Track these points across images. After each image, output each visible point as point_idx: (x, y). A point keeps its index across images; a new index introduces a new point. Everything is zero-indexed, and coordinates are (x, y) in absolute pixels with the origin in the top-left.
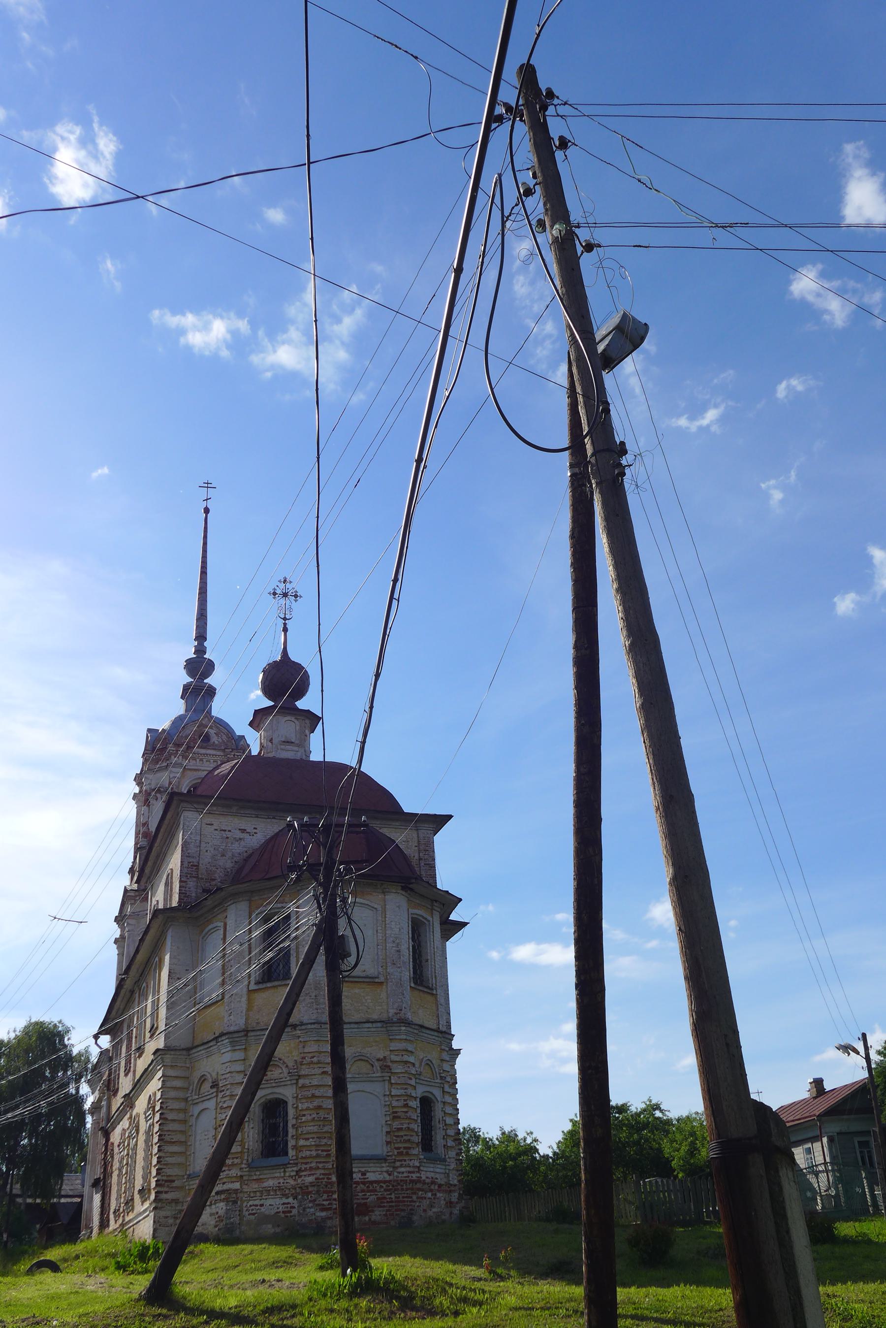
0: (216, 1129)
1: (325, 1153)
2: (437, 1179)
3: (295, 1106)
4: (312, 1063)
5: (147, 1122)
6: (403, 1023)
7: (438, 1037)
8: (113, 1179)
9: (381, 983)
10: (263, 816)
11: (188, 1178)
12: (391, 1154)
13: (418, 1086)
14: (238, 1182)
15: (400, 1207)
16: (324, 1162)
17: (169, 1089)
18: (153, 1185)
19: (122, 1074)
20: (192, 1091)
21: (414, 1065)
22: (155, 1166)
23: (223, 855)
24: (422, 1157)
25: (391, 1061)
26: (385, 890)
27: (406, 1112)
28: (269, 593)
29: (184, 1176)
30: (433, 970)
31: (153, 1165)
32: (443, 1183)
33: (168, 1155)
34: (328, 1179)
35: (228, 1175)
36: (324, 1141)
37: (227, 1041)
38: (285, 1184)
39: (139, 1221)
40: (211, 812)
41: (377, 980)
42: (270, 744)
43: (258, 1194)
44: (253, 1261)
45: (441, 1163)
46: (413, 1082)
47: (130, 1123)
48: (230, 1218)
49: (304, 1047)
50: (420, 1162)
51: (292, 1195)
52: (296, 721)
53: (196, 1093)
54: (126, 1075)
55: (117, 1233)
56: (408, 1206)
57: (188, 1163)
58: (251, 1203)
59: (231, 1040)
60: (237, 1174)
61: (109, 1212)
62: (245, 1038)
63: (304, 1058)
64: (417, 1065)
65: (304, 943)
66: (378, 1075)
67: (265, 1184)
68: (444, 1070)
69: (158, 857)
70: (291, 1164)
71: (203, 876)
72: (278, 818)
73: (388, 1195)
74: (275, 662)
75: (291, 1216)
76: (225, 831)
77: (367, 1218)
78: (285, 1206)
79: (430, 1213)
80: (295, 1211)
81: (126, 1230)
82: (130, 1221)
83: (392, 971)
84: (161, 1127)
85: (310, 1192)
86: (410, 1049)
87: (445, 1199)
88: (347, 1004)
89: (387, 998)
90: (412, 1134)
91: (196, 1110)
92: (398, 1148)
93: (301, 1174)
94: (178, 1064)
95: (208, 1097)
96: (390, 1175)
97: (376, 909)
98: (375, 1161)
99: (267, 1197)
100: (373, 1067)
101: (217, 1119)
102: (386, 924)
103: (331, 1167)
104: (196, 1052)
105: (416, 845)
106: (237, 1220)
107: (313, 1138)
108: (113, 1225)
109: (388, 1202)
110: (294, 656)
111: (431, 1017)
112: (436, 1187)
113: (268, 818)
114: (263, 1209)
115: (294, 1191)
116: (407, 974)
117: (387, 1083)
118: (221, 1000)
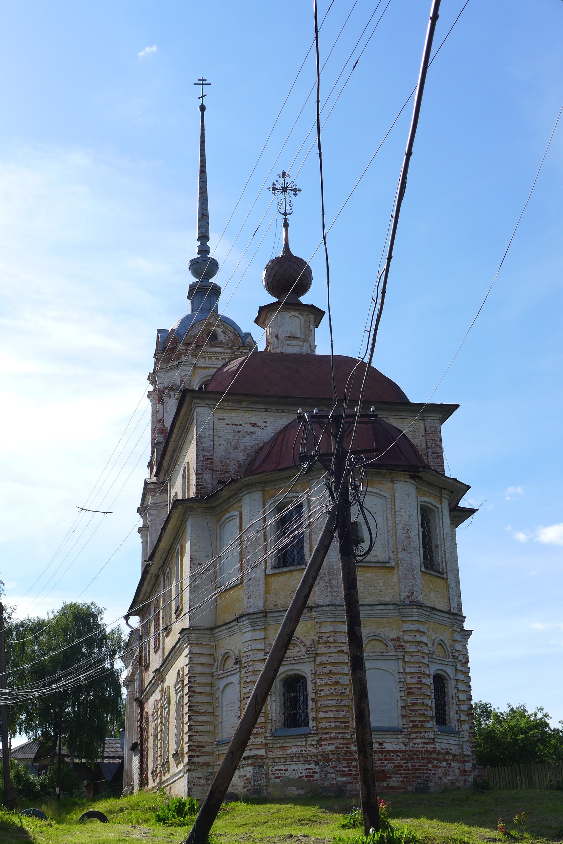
0: (240, 701)
2: (451, 749)
4: (328, 642)
5: (177, 694)
6: (415, 605)
8: (149, 744)
9: (393, 568)
11: (217, 744)
12: (406, 726)
17: (196, 665)
18: (186, 749)
19: (152, 651)
20: (217, 667)
21: (426, 644)
22: (186, 733)
23: (236, 449)
24: (437, 730)
25: (404, 641)
26: (393, 479)
27: (420, 688)
28: (269, 189)
32: (456, 753)
33: (198, 724)
34: (347, 748)
35: (254, 742)
36: (342, 714)
37: (247, 621)
38: (307, 752)
39: (175, 781)
41: (388, 565)
43: (282, 760)
44: (280, 818)
45: (456, 735)
46: (426, 661)
47: (162, 694)
49: (320, 627)
51: (314, 761)
52: (300, 316)
53: (220, 669)
54: (156, 652)
55: (155, 791)
56: (424, 773)
57: (217, 732)
58: (276, 768)
59: (251, 621)
60: (262, 742)
61: (147, 772)
62: (264, 619)
64: (430, 645)
66: (391, 654)
67: (288, 751)
69: (174, 451)
70: (312, 734)
71: (218, 469)
73: (404, 763)
75: (314, 780)
76: (236, 425)
77: (385, 784)
78: (308, 771)
79: (445, 780)
80: (317, 776)
81: (164, 788)
82: (167, 780)
83: (402, 556)
84: (190, 699)
85: (331, 760)
86: (422, 630)
91: (222, 684)
93: (321, 743)
94: (203, 643)
95: (232, 673)
96: (406, 745)
97: (385, 497)
98: (392, 733)
99: (291, 763)
101: (242, 693)
102: (395, 512)
103: (349, 737)
104: (220, 632)
105: (423, 434)
106: (264, 782)
107: (332, 711)
108: (151, 784)
109: (404, 770)
112: (451, 757)
113: (277, 412)
114: (287, 774)
115: (315, 759)
116: (417, 559)
117: (400, 661)
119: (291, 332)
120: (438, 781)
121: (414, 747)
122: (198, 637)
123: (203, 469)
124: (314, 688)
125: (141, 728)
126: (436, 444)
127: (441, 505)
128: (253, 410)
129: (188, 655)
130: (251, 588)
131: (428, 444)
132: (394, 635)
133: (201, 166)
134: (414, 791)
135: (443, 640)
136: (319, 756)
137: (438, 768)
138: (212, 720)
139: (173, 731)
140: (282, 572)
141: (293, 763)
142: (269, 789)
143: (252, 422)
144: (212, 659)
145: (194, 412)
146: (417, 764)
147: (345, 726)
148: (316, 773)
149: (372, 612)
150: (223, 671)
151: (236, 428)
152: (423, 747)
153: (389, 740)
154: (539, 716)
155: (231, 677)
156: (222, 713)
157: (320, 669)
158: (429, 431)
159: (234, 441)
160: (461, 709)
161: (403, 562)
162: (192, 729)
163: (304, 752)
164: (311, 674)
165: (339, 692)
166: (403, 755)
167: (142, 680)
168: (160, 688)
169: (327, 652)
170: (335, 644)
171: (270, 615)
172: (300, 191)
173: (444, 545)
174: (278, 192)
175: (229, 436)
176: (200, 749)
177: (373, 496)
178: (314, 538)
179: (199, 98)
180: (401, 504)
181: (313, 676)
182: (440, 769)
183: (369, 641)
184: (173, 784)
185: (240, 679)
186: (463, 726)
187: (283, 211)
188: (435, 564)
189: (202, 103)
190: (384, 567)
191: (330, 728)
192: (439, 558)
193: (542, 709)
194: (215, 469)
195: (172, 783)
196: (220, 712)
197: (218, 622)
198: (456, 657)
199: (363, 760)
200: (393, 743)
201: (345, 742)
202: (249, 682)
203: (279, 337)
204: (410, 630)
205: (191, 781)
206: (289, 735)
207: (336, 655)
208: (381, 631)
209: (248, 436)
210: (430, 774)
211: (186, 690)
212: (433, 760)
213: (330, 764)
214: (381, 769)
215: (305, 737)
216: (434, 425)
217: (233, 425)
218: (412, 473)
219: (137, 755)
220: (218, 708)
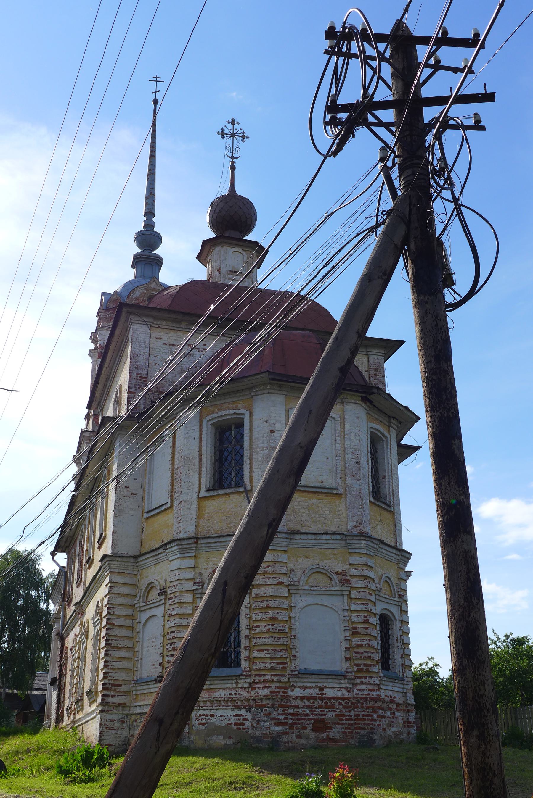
0: (164, 636)
1: (281, 666)
2: (395, 697)
4: (267, 573)
6: (363, 536)
7: (397, 555)
8: (67, 679)
9: (340, 495)
11: (135, 683)
12: (350, 670)
13: (378, 603)
17: (117, 596)
18: (100, 688)
19: (75, 585)
20: (140, 599)
21: (373, 580)
22: (102, 670)
24: (382, 675)
25: (351, 576)
26: (344, 400)
27: (367, 628)
28: (218, 133)
29: (131, 681)
30: (391, 487)
31: (100, 668)
32: (401, 702)
33: (115, 659)
34: (284, 692)
36: (279, 654)
37: (176, 547)
38: (237, 696)
39: (88, 721)
40: (161, 326)
41: (335, 492)
42: (218, 273)
43: (208, 704)
44: (208, 779)
45: (400, 682)
46: (373, 598)
47: (81, 628)
50: (379, 680)
51: (245, 707)
52: (243, 253)
53: (143, 600)
54: (78, 586)
55: (68, 729)
56: (369, 724)
57: (135, 669)
58: (201, 712)
59: (180, 547)
61: (63, 708)
62: (195, 545)
64: (377, 581)
65: (258, 450)
66: (336, 589)
67: (215, 694)
68: (401, 589)
69: (107, 379)
70: (244, 675)
74: (223, 196)
75: (244, 729)
77: (325, 735)
78: (237, 717)
79: (389, 732)
80: (247, 724)
81: (77, 727)
82: (80, 719)
83: (351, 483)
84: (108, 632)
85: (265, 706)
86: (370, 564)
87: (403, 719)
88: (304, 514)
89: (346, 511)
90: (372, 651)
91: (144, 617)
92: (357, 665)
93: (254, 686)
94: (126, 571)
95: (156, 604)
96: (349, 692)
97: (334, 418)
98: (334, 677)
99: (218, 707)
100: (331, 580)
101: (166, 627)
102: (344, 435)
103: (287, 680)
105: (366, 369)
107: (268, 650)
108: (66, 721)
109: (346, 720)
110: (239, 191)
111: (389, 534)
112: (395, 706)
114: (213, 720)
115: (246, 704)
116: (366, 487)
117: (346, 597)
119: (233, 267)
120: (382, 733)
123: (135, 387)
124: (248, 624)
125: (60, 663)
126: (378, 380)
127: (390, 435)
129: (108, 584)
130: (182, 512)
131: (371, 379)
132: (340, 569)
133: (151, 152)
134: (357, 744)
135: (389, 576)
136: (250, 701)
137: (382, 718)
138: (131, 656)
139: (89, 666)
140: (217, 495)
141: (221, 707)
142: (192, 736)
144: (135, 589)
145: (130, 329)
146: (361, 714)
147: (282, 667)
148: (246, 720)
149: (317, 541)
150: (146, 602)
152: (369, 694)
154: (430, 665)
156: (142, 649)
157: (257, 603)
158: (373, 367)
160: (406, 653)
161: (352, 489)
162: (109, 665)
163: (234, 696)
164: (246, 608)
165: (276, 629)
167: (64, 616)
168: (79, 622)
169: (265, 583)
170: (275, 576)
171: (202, 541)
172: (248, 138)
173: (392, 477)
174: (226, 136)
176: (116, 687)
178: (255, 459)
179: (153, 93)
180: (351, 428)
181: (248, 611)
182: (385, 719)
183: (312, 573)
184: (86, 724)
185: (164, 612)
186: (407, 671)
187: (230, 155)
188: (382, 496)
189: (156, 97)
190: (331, 493)
191: (265, 670)
192: (385, 490)
193: (433, 659)
195: (85, 723)
196: (140, 648)
197: (143, 550)
198: (402, 597)
199: (479, 747)
200: (335, 689)
201: (282, 685)
202: (175, 615)
203: (221, 271)
204: (358, 563)
205: (103, 724)
207: (275, 588)
208: (325, 563)
210: (375, 725)
211: (104, 622)
212: (378, 709)
213: (264, 710)
214: (320, 717)
215: (235, 679)
216: (378, 361)
217: (170, 345)
218: (364, 395)
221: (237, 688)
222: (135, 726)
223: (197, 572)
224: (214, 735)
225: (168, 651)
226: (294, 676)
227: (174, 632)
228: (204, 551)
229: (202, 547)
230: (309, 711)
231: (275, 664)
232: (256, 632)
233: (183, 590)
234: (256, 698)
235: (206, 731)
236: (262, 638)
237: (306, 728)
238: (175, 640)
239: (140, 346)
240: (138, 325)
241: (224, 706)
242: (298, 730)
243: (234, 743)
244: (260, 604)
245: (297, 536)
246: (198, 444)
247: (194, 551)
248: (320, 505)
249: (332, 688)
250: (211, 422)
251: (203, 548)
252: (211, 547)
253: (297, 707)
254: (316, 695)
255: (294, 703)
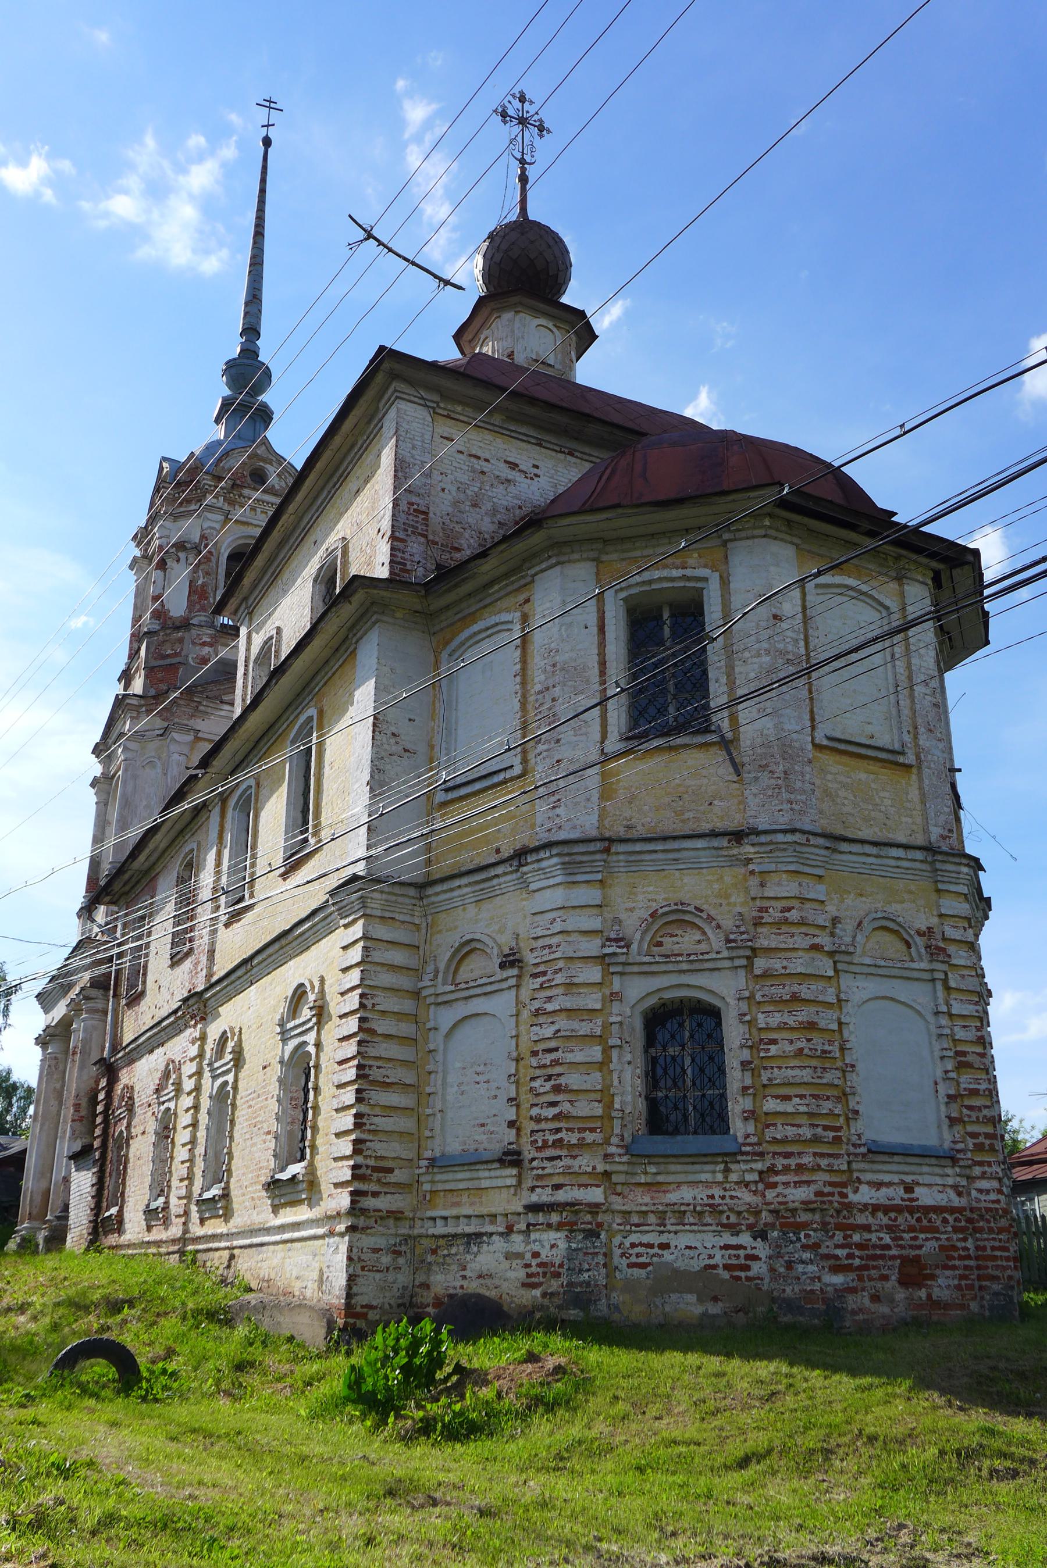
1: (832, 1134)
3: (748, 1018)
5: (284, 1041)
9: (908, 767)
10: (551, 446)
12: (961, 1146)
14: (597, 1186)
15: (990, 1270)
16: (830, 1155)
17: (378, 968)
20: (436, 977)
23: (475, 505)
33: (377, 1111)
35: (570, 1167)
36: (826, 1106)
37: (555, 860)
38: (728, 1201)
40: (453, 415)
48: (581, 1271)
49: (762, 885)
51: (750, 1227)
52: (555, 330)
54: (176, 961)
58: (634, 1238)
59: (567, 859)
60: (594, 1168)
62: (605, 856)
63: (763, 910)
66: (924, 965)
69: (281, 545)
70: (747, 1153)
71: (437, 539)
72: (579, 455)
73: (959, 1240)
75: (748, 1278)
76: (478, 458)
77: (923, 1293)
78: (730, 1252)
80: (758, 1268)
84: (363, 1049)
85: (805, 1225)
88: (846, 802)
91: (445, 1018)
92: (974, 1135)
93: (771, 1180)
94: (397, 916)
95: (489, 989)
96: (959, 1194)
97: (887, 608)
98: (933, 1161)
99: (679, 1228)
103: (845, 1167)
104: (445, 892)
106: (600, 1276)
107: (802, 1097)
109: (961, 1258)
113: (561, 452)
114: (667, 1256)
117: (939, 986)
118: (519, 777)
121: (978, 1200)
122: (386, 901)
123: (406, 530)
124: (747, 1036)
128: (513, 434)
134: (987, 1313)
141: (687, 1227)
142: (614, 1294)
143: (509, 459)
146: (988, 1244)
148: (756, 1258)
150: (456, 985)
151: (479, 465)
153: (927, 1179)
155: (482, 999)
156: (444, 1089)
157: (766, 988)
159: (471, 488)
162: (365, 1124)
163: (718, 1201)
165: (816, 1050)
166: (955, 1220)
169: (783, 946)
170: (804, 929)
172: (549, 131)
175: (465, 478)
176: (381, 1175)
177: (862, 604)
178: (741, 673)
181: (744, 1006)
183: (874, 929)
185: (517, 1004)
191: (798, 1141)
194: (431, 537)
202: (554, 1012)
205: (356, 1258)
206: (675, 1152)
207: (807, 956)
209: (501, 487)
213: (802, 1236)
217: (471, 455)
219: (88, 1170)
220: (433, 1076)
221: (727, 1182)
222: (430, 1263)
223: (609, 916)
224: (673, 1292)
225: (537, 1095)
226: (860, 1158)
227: (556, 1049)
228: (622, 870)
229: (618, 861)
230: (891, 1238)
231: (819, 1130)
232: (770, 1054)
233: (575, 955)
234: (782, 1207)
235: (649, 1282)
236: (787, 1068)
237: (885, 1278)
238: (557, 1070)
239: (414, 447)
240: (409, 404)
241: (695, 1224)
242: (872, 1283)
243: (725, 1313)
244: (775, 991)
245: (844, 847)
246: (595, 640)
247: (600, 869)
248: (873, 786)
249: (930, 1185)
250: (623, 594)
251: (622, 864)
252: (642, 861)
253: (867, 1228)
254: (901, 1202)
255: (861, 1219)
